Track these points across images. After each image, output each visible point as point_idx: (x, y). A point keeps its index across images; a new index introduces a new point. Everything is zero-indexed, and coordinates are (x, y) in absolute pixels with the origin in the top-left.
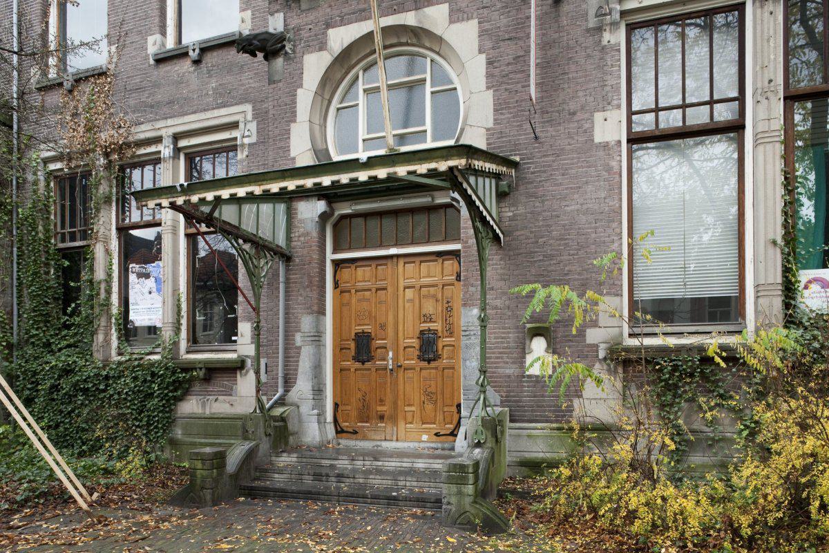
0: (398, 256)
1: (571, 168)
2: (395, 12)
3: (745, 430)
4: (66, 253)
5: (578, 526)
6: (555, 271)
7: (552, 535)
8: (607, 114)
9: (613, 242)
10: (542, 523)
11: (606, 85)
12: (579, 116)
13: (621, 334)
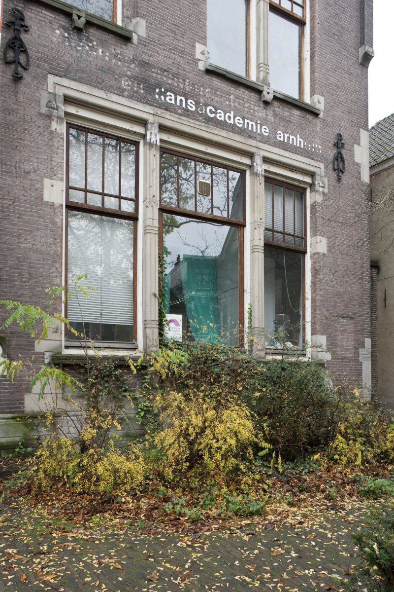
1: (25, 215)
3: (141, 412)
5: (52, 493)
6: (10, 293)
7: (35, 504)
8: (54, 182)
9: (56, 277)
10: (20, 496)
11: (53, 160)
12: (32, 176)
13: (61, 346)
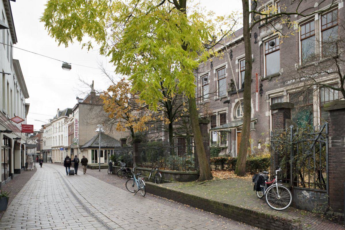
12: (264, 112)
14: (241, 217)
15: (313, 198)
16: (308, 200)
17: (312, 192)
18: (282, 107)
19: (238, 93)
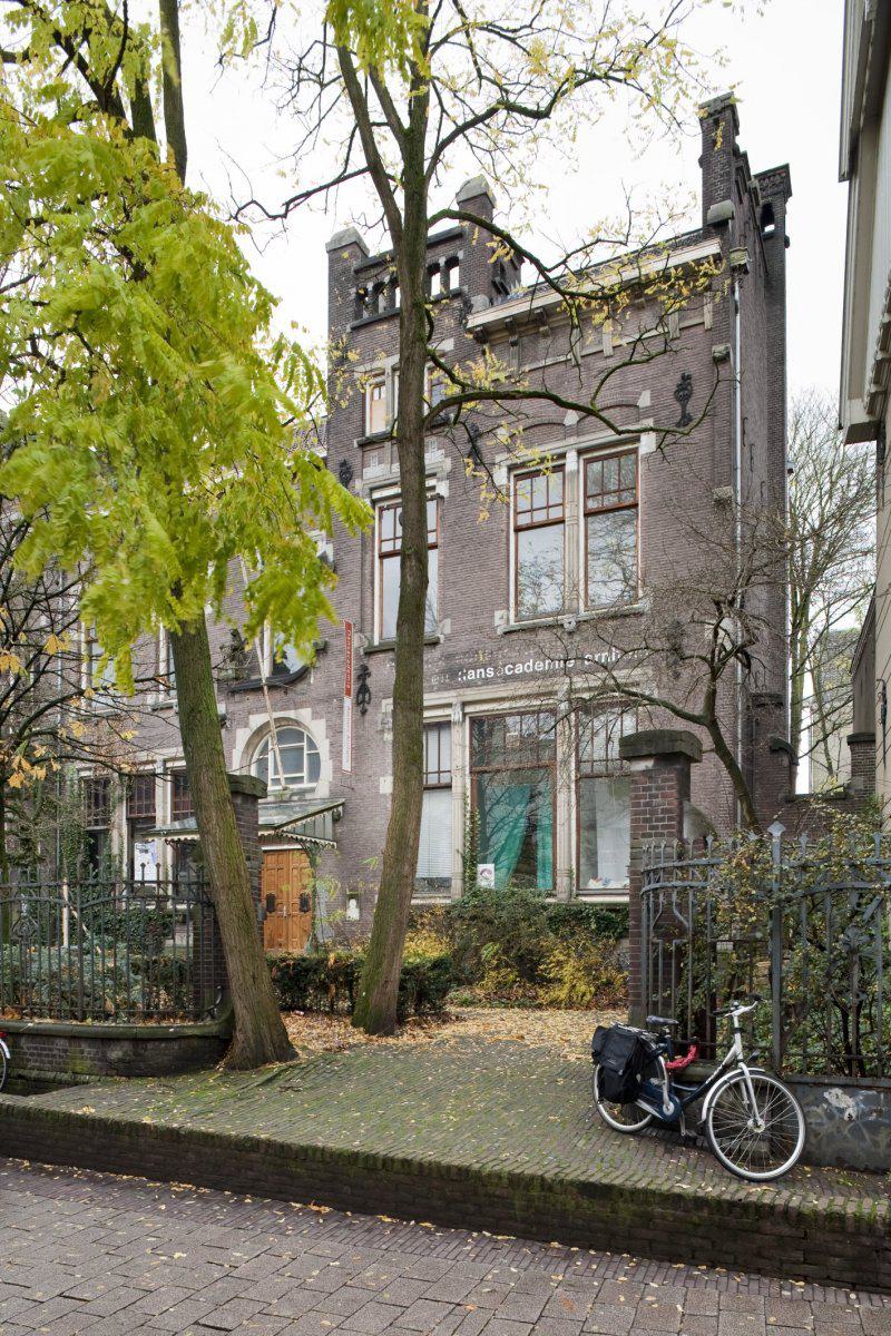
0: (289, 850)
2: (285, 709)
4: (92, 834)
14: (696, 1242)
15: (873, 1117)
16: (852, 1124)
17: (870, 1093)
18: (677, 750)
19: (265, 688)
